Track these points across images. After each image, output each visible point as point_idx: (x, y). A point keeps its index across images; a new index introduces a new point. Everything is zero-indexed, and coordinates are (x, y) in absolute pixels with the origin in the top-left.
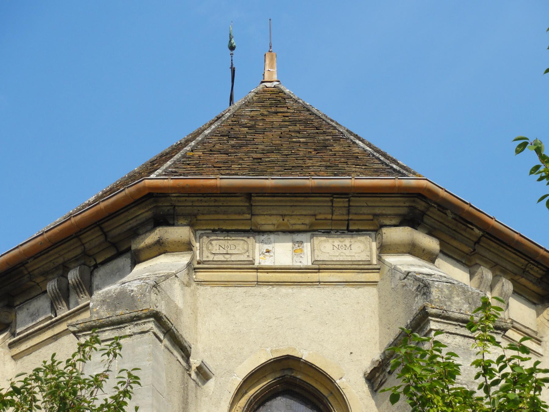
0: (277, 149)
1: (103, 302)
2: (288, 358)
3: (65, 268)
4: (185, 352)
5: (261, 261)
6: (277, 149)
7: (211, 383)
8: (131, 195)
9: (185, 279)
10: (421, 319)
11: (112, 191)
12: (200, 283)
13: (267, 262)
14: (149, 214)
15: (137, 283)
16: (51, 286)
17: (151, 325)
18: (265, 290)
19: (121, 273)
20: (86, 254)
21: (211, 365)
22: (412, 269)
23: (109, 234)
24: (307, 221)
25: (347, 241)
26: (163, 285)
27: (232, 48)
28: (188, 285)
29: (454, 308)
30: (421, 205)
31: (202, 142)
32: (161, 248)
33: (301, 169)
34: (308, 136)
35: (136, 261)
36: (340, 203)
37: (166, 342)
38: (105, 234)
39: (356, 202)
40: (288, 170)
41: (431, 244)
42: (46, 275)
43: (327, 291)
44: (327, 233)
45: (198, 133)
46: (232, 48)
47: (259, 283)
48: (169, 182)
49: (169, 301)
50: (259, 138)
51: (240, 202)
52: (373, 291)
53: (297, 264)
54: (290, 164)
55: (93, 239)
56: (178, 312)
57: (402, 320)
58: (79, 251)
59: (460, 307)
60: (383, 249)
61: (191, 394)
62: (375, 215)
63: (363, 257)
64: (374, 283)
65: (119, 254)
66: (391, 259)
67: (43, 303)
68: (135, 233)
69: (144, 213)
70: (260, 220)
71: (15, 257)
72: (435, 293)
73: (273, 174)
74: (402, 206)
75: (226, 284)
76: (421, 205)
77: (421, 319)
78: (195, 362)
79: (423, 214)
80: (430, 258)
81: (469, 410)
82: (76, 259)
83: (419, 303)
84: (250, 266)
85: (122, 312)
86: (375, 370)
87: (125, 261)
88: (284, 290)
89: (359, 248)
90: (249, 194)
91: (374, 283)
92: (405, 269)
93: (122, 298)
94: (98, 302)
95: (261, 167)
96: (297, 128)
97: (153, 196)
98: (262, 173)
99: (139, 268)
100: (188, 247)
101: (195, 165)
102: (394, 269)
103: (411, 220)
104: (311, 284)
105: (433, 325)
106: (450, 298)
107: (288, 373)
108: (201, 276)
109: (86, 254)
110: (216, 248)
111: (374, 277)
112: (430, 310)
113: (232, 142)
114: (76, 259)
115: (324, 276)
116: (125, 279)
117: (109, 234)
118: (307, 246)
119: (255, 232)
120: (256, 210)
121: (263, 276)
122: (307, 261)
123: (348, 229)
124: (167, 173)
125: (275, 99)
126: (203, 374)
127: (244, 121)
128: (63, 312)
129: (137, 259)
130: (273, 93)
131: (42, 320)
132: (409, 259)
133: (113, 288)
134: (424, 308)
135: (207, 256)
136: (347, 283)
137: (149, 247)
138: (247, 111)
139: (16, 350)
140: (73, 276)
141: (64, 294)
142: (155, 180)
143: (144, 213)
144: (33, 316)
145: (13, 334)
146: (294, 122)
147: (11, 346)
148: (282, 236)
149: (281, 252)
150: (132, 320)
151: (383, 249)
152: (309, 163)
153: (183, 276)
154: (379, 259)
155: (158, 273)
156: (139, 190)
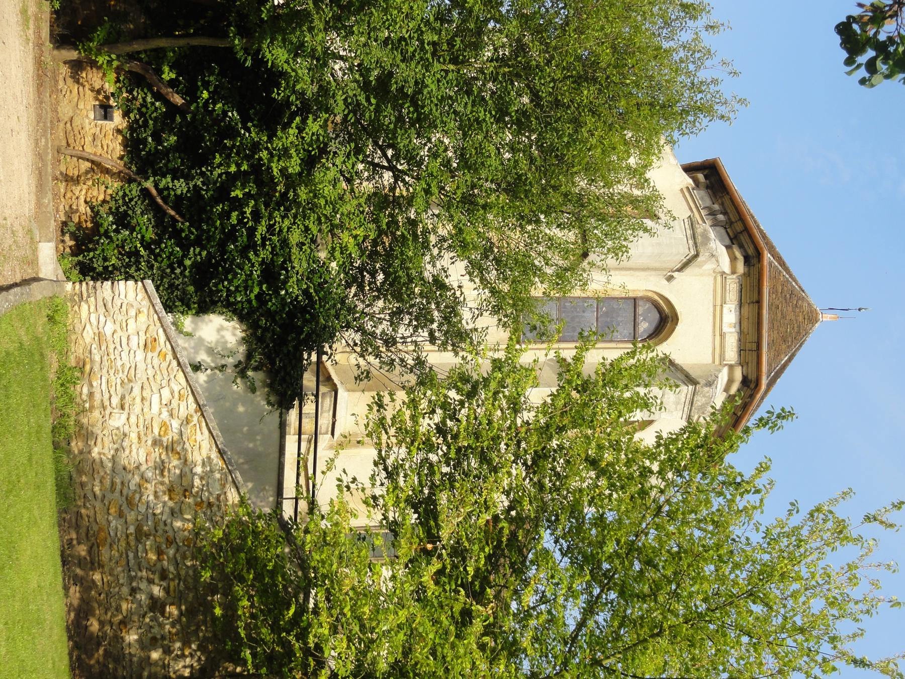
0: (784, 317)
1: (705, 230)
2: (678, 319)
3: (725, 213)
4: (680, 270)
5: (726, 308)
6: (784, 317)
7: (666, 282)
8: (760, 244)
9: (717, 271)
10: (690, 380)
11: (764, 236)
12: (715, 278)
13: (725, 310)
14: (750, 253)
15: (714, 247)
16: (716, 207)
17: (693, 253)
18: (711, 309)
19: (721, 241)
20: (731, 223)
21: (674, 282)
22: (720, 379)
23: (741, 233)
24: (746, 330)
25: (735, 349)
26: (713, 259)
27: (860, 310)
28: (714, 272)
29: (699, 398)
30: (752, 386)
31: (788, 281)
32: (733, 259)
33: (771, 328)
34: (790, 333)
35: (727, 247)
36: (754, 346)
37: (685, 260)
38: (741, 232)
39: (755, 354)
40: (772, 322)
41: (734, 390)
42: (722, 204)
43: (710, 339)
44: (740, 340)
45: (795, 280)
46: (860, 310)
47: (715, 306)
48: (766, 263)
49: (705, 262)
50: (790, 309)
51: (755, 298)
52: (710, 361)
53: (724, 325)
54: (775, 323)
55: (739, 227)
56: (700, 266)
57: (693, 374)
58: (733, 220)
59: (699, 400)
60: (731, 367)
61: (660, 272)
62: (748, 363)
63: (727, 357)
64: (714, 362)
65: (731, 239)
66: (725, 370)
67: (708, 203)
68: (741, 246)
69: (751, 251)
70: (747, 306)
71: (731, 189)
72: (706, 389)
73: (770, 314)
74: (752, 376)
75: (715, 291)
76: (752, 386)
77: (690, 380)
78: (676, 274)
79: (748, 387)
80: (727, 389)
81: (155, 4)
82: (729, 219)
83: (702, 382)
84: (724, 302)
85: (699, 239)
86: (671, 363)
87: (728, 242)
88: (711, 318)
89: (732, 355)
90: (759, 302)
91: (714, 362)
92: (720, 376)
93: (707, 239)
94: (705, 226)
95: (773, 308)
96: (796, 329)
97: (759, 255)
98: (770, 308)
99: (724, 249)
100: (733, 272)
101: (774, 278)
102: (720, 371)
103: (745, 381)
104: (714, 332)
105: (691, 387)
106: (704, 396)
107: (670, 320)
108: (719, 278)
109: (731, 223)
110: (733, 286)
111: (717, 362)
112: (698, 386)
113: (788, 296)
114: (729, 219)
115: (718, 338)
116: (717, 241)
117: (741, 233)
118: (733, 330)
119: (741, 305)
120: (751, 305)
121: (718, 308)
122: (725, 329)
123: (741, 350)
124: (770, 264)
125: (812, 318)
126: (670, 279)
127: (800, 302)
128: (703, 213)
129: (728, 247)
130: (816, 318)
131: (700, 202)
132: (726, 379)
133: (712, 235)
134: (698, 383)
135: (728, 282)
136: (714, 349)
137: (734, 253)
138: (805, 304)
139: (685, 190)
140: (721, 217)
141: (712, 213)
142: (767, 256)
143: (751, 251)
144: (702, 199)
145: (693, 189)
146: (799, 327)
147: (688, 188)
148: (738, 318)
149: (730, 316)
150: (695, 243)
151: (731, 367)
152: (776, 332)
153: (719, 269)
154: (726, 365)
155: (720, 256)
156: (762, 248)
